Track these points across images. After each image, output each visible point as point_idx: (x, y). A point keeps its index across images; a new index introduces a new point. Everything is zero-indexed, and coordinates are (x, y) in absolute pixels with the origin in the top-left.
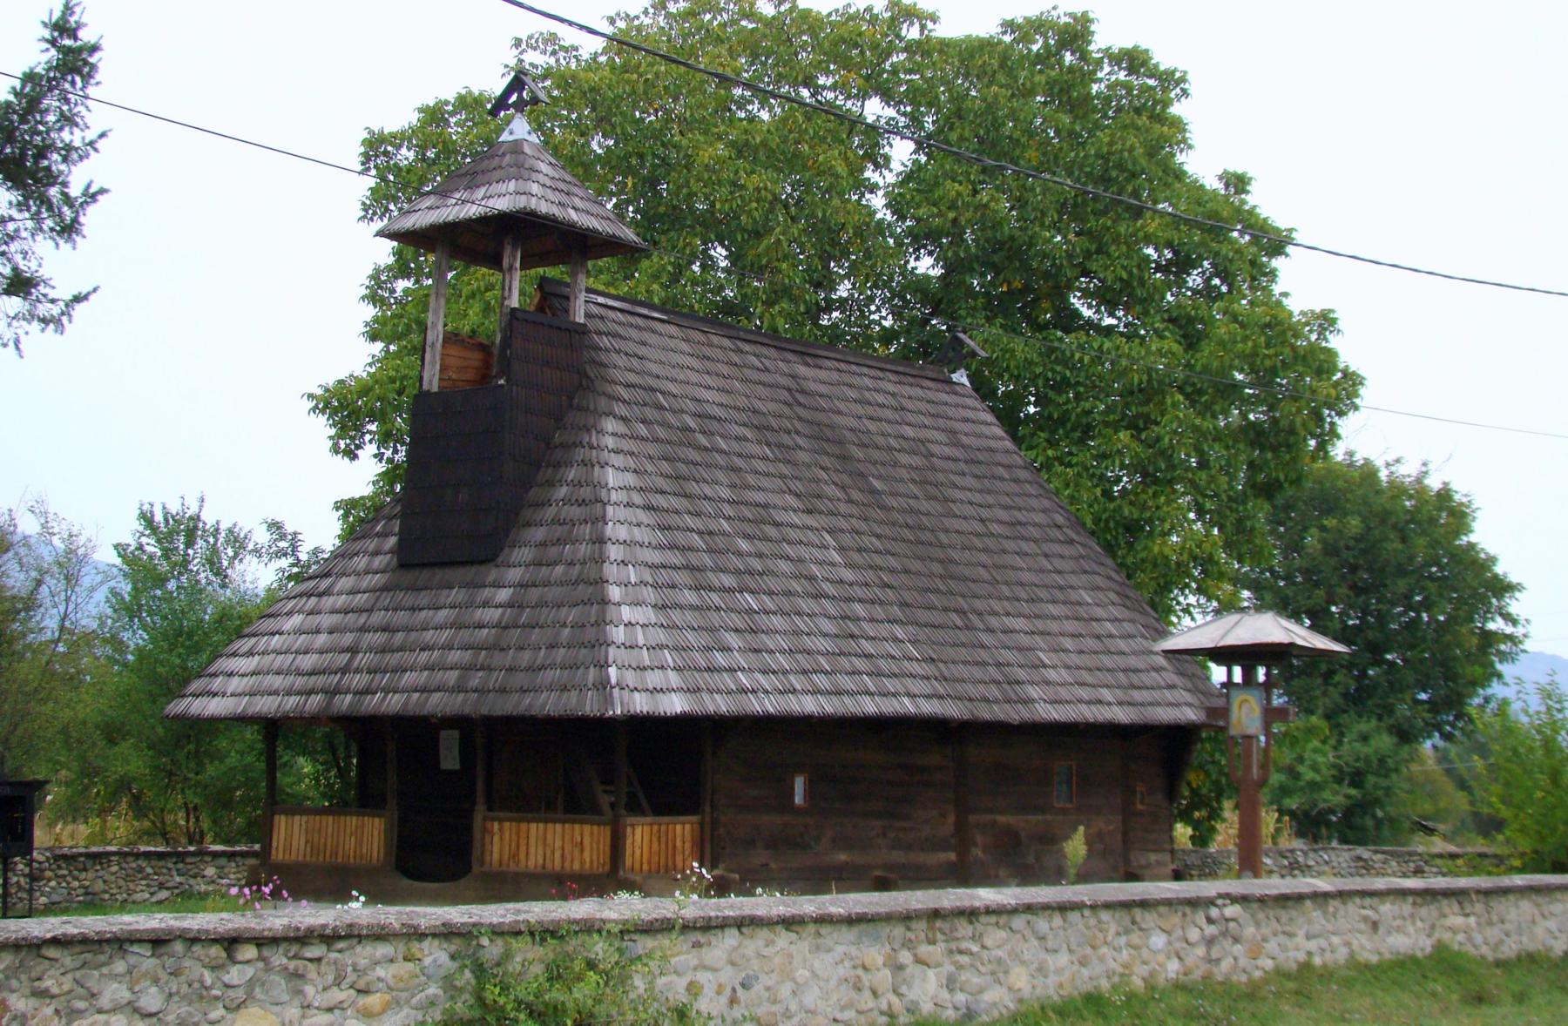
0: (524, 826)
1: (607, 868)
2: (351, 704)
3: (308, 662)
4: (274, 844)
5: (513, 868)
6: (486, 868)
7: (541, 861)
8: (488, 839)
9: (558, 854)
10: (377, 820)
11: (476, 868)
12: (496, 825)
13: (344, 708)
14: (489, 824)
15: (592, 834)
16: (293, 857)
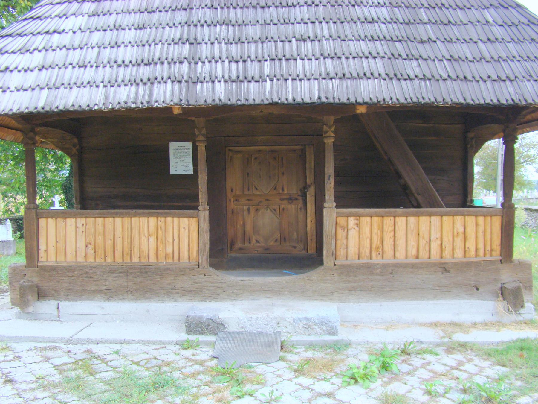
0: (389, 221)
1: (496, 256)
2: (229, 93)
3: (128, 54)
4: (42, 247)
5: (376, 259)
6: (341, 261)
7: (414, 252)
8: (341, 233)
9: (435, 246)
10: (184, 221)
11: (328, 260)
12: (352, 221)
13: (41, 104)
14: (341, 221)
15: (477, 224)
16: (70, 258)
